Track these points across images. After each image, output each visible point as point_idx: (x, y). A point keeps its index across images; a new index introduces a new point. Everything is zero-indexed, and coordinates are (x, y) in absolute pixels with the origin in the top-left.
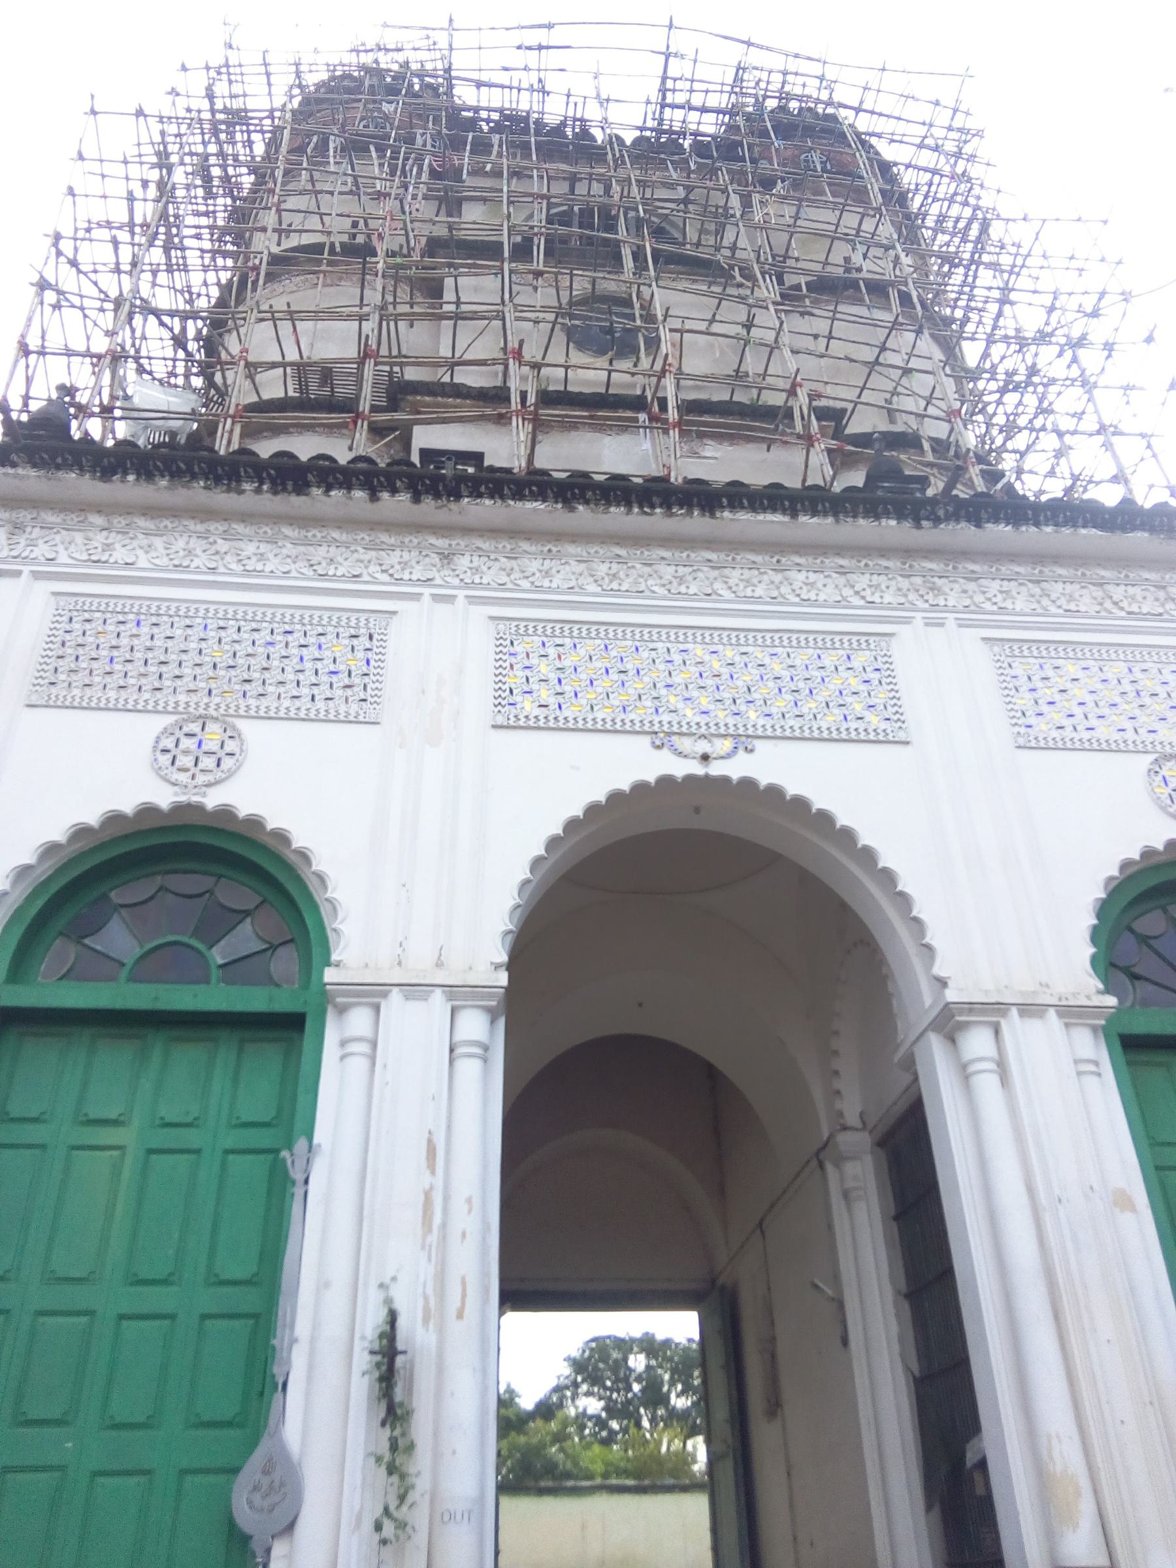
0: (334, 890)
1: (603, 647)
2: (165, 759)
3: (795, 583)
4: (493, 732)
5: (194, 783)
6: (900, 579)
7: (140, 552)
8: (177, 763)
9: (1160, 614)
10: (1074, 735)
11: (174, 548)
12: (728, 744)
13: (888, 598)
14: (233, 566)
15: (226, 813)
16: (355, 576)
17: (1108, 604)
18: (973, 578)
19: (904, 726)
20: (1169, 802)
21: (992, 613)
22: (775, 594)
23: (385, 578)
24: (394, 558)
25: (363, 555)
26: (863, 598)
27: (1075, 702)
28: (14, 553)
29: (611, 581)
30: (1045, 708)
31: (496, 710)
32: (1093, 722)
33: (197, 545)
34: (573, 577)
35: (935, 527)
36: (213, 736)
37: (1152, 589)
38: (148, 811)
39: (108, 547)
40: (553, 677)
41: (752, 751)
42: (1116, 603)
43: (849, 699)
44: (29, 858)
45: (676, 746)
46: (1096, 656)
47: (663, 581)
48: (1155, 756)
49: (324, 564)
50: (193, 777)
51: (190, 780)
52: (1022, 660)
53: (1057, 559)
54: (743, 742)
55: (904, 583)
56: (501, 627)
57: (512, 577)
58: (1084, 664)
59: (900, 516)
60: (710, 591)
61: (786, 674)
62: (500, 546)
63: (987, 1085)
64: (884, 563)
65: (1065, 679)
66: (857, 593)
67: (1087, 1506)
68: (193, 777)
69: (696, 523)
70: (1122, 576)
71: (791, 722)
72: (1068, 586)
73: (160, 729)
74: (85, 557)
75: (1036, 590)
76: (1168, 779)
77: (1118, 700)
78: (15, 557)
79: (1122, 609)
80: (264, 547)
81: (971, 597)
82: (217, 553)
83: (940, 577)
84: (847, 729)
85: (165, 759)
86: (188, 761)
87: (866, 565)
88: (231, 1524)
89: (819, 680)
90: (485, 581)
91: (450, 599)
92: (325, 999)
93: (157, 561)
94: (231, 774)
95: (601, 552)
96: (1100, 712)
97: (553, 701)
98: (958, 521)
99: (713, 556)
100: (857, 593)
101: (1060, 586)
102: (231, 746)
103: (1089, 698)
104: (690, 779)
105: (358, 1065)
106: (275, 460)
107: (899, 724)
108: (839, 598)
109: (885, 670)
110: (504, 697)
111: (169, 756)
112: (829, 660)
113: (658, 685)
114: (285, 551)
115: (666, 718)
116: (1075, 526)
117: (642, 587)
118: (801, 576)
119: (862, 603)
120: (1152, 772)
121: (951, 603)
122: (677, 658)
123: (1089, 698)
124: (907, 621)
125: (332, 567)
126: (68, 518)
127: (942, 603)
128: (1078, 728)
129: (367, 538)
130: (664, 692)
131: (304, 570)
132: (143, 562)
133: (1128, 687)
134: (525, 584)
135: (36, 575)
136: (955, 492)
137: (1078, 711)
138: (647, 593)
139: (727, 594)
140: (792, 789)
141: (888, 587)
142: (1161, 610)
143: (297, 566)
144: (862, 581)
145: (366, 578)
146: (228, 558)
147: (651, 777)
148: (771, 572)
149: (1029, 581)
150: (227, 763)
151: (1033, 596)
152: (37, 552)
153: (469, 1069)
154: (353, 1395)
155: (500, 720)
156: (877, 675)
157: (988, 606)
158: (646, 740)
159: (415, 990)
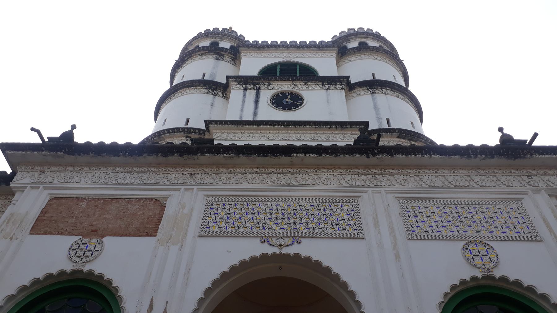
0: (125, 303)
1: (246, 204)
2: (73, 253)
3: (322, 179)
4: (199, 238)
5: (81, 262)
6: (363, 176)
7: (82, 179)
8: (77, 254)
9: (468, 186)
10: (432, 234)
11: (94, 177)
12: (291, 240)
13: (358, 183)
14: (114, 182)
15: (91, 273)
16: (157, 183)
17: (447, 183)
18: (392, 175)
19: (362, 232)
20: (472, 260)
21: (400, 188)
22: (314, 183)
23: (168, 183)
25: (162, 175)
26: (348, 183)
27: (432, 221)
28: (39, 181)
29: (252, 181)
30: (421, 224)
31: (201, 230)
32: (441, 229)
33: (103, 175)
34: (238, 180)
35: (375, 156)
37: (465, 177)
38: (62, 273)
39: (72, 177)
40: (225, 216)
41: (300, 243)
42: (450, 183)
43: (341, 222)
44: (13, 292)
45: (270, 242)
46: (417, 202)
47: (272, 180)
48: (466, 242)
49: (147, 179)
50: (82, 260)
51: (80, 261)
52: (412, 205)
53: (426, 167)
54: (297, 240)
55: (365, 178)
56: (209, 199)
57: (215, 181)
58: (437, 206)
59: (361, 154)
60: (289, 182)
61: (316, 213)
62: (487, 171)
64: (357, 170)
65: (429, 212)
66: (346, 182)
68: (82, 260)
69: (285, 159)
70: (452, 172)
71: (317, 231)
72: (430, 177)
73: (74, 241)
74: (63, 181)
75: (417, 179)
76: (471, 251)
77: (451, 219)
78: (38, 182)
79: (452, 184)
80: (126, 175)
81: (391, 182)
82: (109, 177)
83: (379, 175)
84: (339, 233)
85: (73, 253)
86: (80, 253)
87: (350, 171)
89: (329, 214)
90: (205, 182)
93: (87, 182)
94: (96, 258)
95: (250, 170)
96: (443, 225)
97: (224, 226)
98: (383, 154)
99: (292, 170)
100: (346, 182)
101: (427, 177)
102: (98, 247)
103: (438, 219)
104: (274, 255)
106: (396, 146)
107: (360, 231)
108: (339, 184)
109: (356, 211)
111: (75, 252)
113: (266, 218)
114: (133, 176)
115: (267, 231)
116: (430, 154)
117: (264, 182)
118: (325, 176)
119: (348, 185)
120: (465, 248)
121: (383, 184)
122: (274, 208)
123: (438, 219)
124: (366, 192)
125: (149, 180)
126: (60, 168)
127: (379, 184)
128: (434, 231)
129: (164, 169)
130: (268, 221)
131: (139, 182)
133: (455, 215)
134: (220, 183)
135: (45, 188)
137: (434, 225)
138: (266, 184)
139: (296, 184)
140: (315, 258)
141: (358, 179)
142: (468, 184)
143: (136, 181)
144: (348, 177)
145: (161, 183)
146: (113, 179)
147: (258, 254)
148: (313, 175)
149: (415, 175)
150: (96, 253)
151: (416, 181)
152: (47, 180)
155: (202, 233)
156: (353, 212)
157: (398, 185)
158: (258, 240)
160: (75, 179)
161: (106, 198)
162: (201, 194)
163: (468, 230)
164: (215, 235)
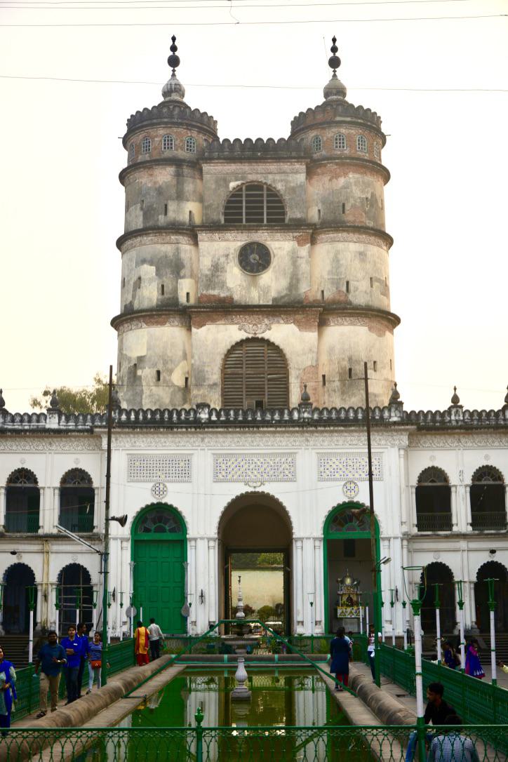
2: (154, 493)
12: (259, 484)
24: (192, 440)
36: (161, 486)
54: (262, 484)
63: (299, 551)
67: (301, 612)
88: (181, 614)
91: (204, 449)
92: (186, 539)
94: (166, 496)
102: (165, 489)
105: (193, 550)
109: (293, 464)
110: (216, 475)
112: (283, 460)
122: (251, 462)
132: (142, 446)
136: (311, 231)
150: (154, 489)
153: (212, 551)
154: (318, 581)
158: (243, 483)
159: (202, 538)
160: (138, 444)
161: (48, 574)
162: (210, 451)
163: (349, 474)
164: (221, 481)
